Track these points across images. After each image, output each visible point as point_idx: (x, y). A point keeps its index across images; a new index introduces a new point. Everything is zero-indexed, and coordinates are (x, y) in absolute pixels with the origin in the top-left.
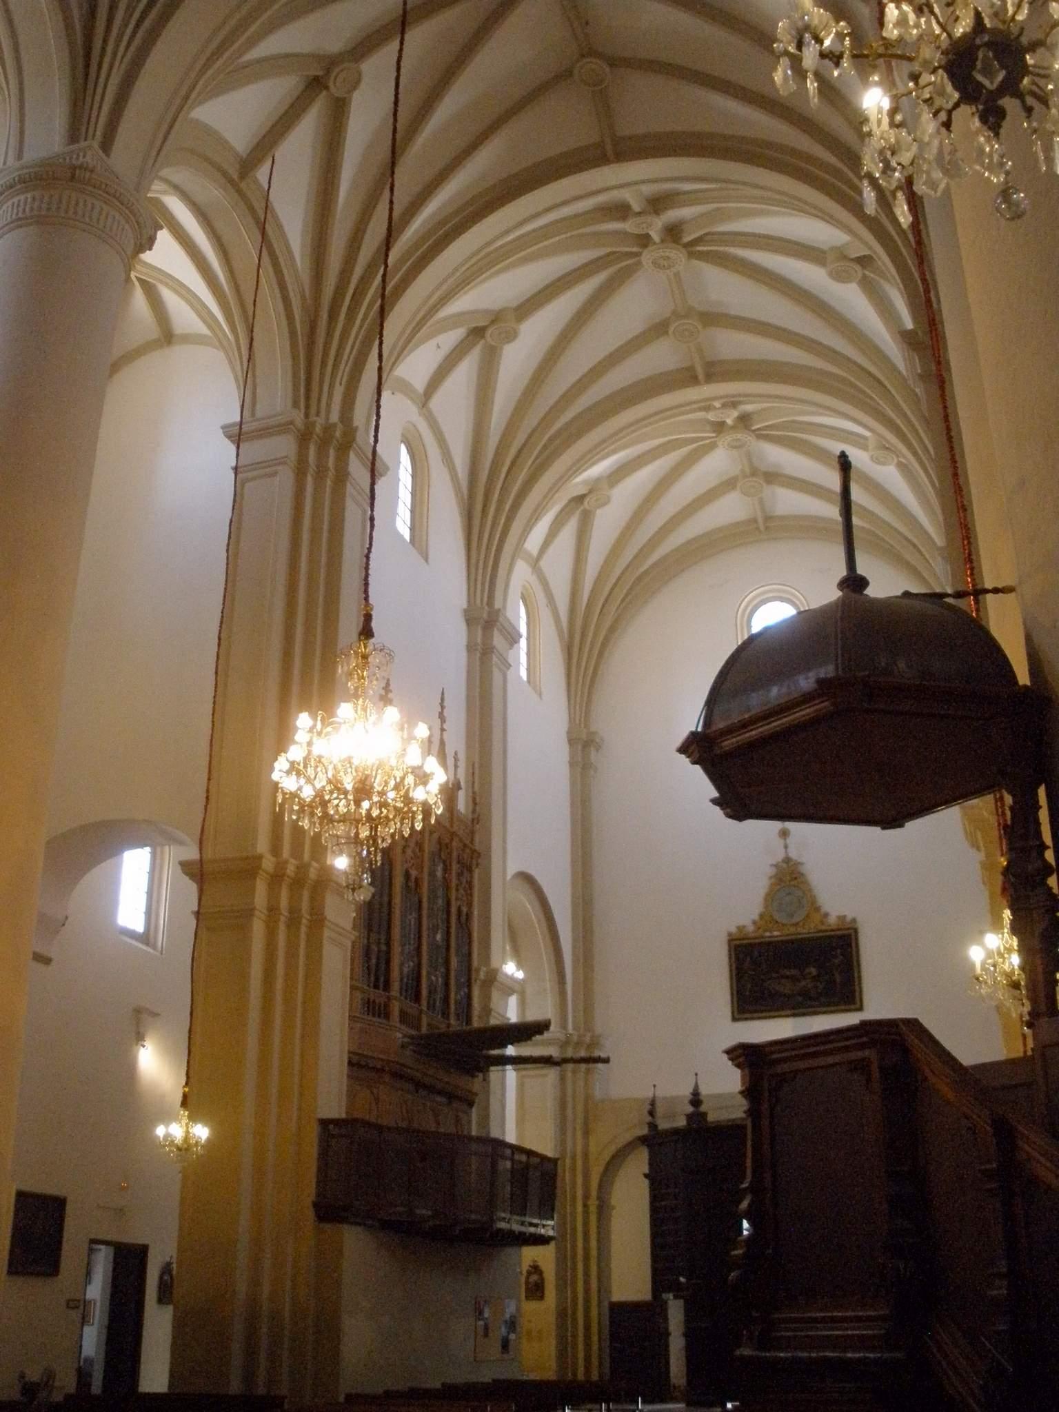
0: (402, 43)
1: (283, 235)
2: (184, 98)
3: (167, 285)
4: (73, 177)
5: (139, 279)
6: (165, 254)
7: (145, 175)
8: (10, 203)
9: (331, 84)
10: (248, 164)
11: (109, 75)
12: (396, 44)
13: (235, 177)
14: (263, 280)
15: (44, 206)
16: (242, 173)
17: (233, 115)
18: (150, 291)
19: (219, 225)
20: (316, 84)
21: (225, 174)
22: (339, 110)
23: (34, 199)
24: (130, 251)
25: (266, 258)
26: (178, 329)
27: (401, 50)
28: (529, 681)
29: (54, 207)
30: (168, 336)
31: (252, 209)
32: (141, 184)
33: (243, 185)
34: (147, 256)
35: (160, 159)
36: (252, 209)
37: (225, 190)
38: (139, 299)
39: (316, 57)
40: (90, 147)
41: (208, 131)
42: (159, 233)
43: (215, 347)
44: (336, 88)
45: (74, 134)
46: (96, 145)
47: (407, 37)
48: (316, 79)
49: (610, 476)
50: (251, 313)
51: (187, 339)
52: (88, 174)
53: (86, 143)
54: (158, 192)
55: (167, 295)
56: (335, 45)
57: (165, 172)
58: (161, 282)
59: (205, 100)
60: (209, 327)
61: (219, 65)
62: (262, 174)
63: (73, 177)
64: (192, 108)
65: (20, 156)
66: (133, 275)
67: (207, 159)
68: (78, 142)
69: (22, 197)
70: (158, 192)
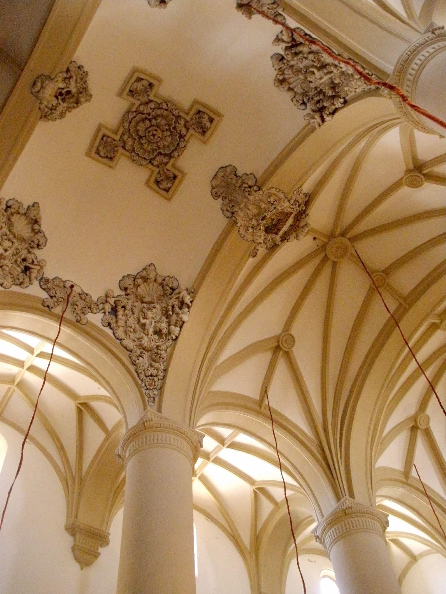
0: (435, 393)
1: (438, 494)
2: (370, 463)
3: (404, 537)
4: (346, 514)
5: (390, 540)
6: (395, 525)
7: (371, 498)
8: (327, 536)
9: (420, 426)
10: (407, 473)
11: (339, 470)
12: (434, 396)
13: (405, 480)
14: (438, 515)
15: (341, 530)
16: (406, 476)
17: (391, 458)
18: (396, 542)
19: (408, 502)
20: (414, 429)
21: (396, 480)
22: (428, 433)
23: (336, 530)
24: (381, 530)
25: (433, 505)
26: (416, 552)
27: (437, 396)
28: (209, 392)
29: (344, 529)
30: (414, 558)
31: (418, 489)
32: (372, 502)
33: (409, 482)
34: (388, 529)
35: (374, 489)
36: (418, 489)
37: (403, 487)
38: (394, 548)
39: (410, 419)
40: (346, 499)
41: (385, 469)
42: (388, 518)
43: (434, 553)
44: (422, 426)
45: (338, 498)
46: (347, 496)
47: (436, 391)
48: (413, 427)
49: (420, 409)
50: (442, 532)
51: (422, 555)
52: (350, 510)
53: (344, 499)
54: (379, 502)
55: (405, 541)
56: (412, 411)
57: (378, 493)
58: (399, 536)
59: (379, 457)
60: (428, 545)
61: (376, 443)
62: (414, 473)
63: (346, 514)
64: (374, 465)
65: (323, 516)
66: (387, 539)
67: (391, 480)
68: (341, 499)
69: (331, 531)
70: (379, 502)
